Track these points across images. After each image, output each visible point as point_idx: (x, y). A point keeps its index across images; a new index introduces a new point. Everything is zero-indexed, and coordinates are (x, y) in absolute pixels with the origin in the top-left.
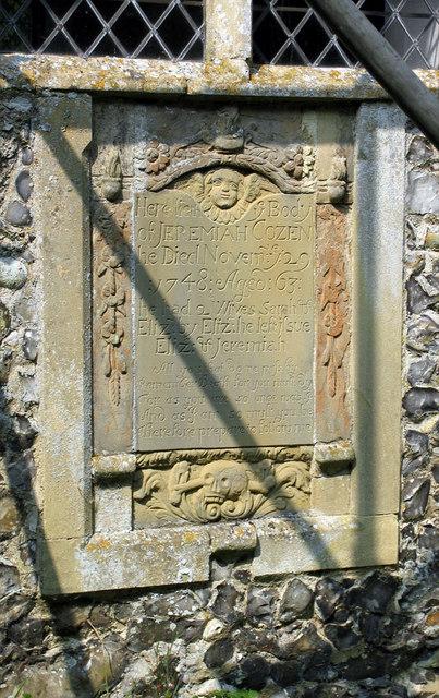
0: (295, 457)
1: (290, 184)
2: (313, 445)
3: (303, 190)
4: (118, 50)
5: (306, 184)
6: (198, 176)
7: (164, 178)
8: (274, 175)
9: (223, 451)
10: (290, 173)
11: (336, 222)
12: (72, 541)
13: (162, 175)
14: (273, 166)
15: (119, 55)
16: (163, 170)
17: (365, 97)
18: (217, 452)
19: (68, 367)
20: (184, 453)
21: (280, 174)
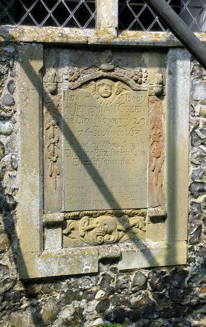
0: (139, 214)
1: (136, 86)
2: (147, 208)
3: (142, 89)
4: (55, 24)
5: (143, 86)
6: (93, 82)
7: (77, 83)
8: (129, 82)
9: (104, 211)
10: (136, 81)
11: (158, 104)
12: (34, 254)
13: (76, 82)
14: (128, 78)
15: (56, 26)
16: (77, 79)
17: (171, 45)
18: (102, 212)
19: (32, 172)
20: (86, 212)
21: (131, 82)
